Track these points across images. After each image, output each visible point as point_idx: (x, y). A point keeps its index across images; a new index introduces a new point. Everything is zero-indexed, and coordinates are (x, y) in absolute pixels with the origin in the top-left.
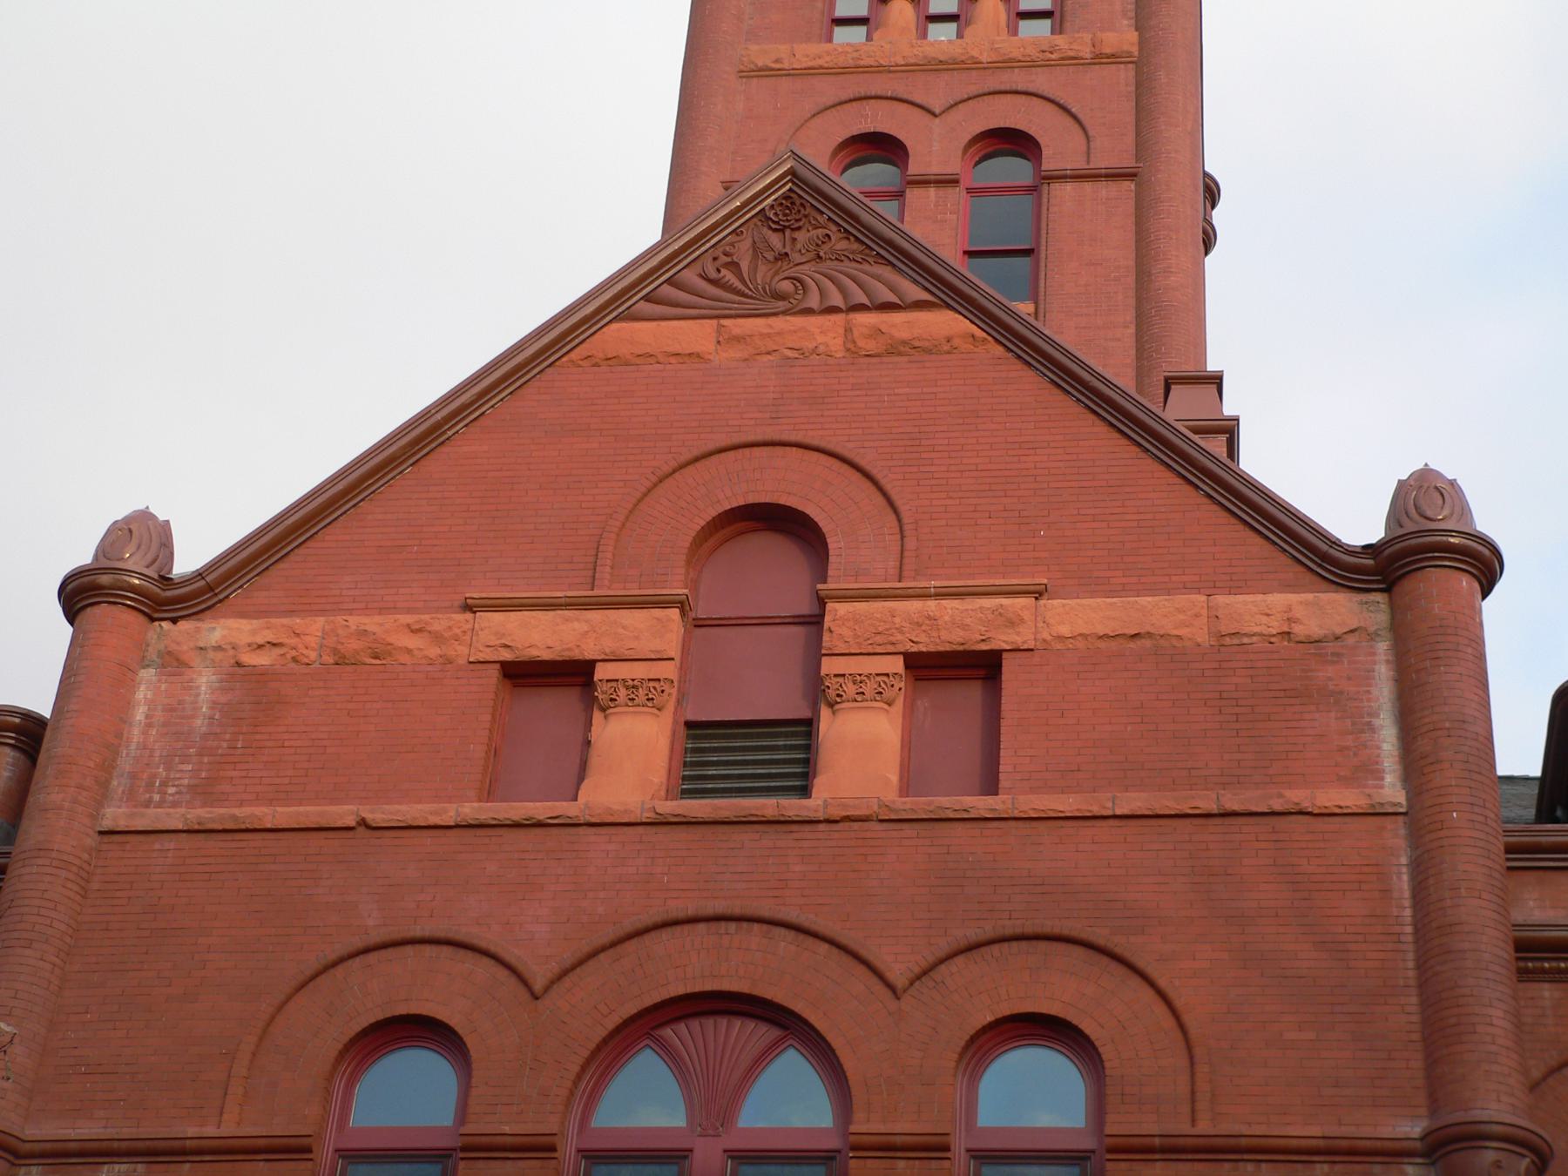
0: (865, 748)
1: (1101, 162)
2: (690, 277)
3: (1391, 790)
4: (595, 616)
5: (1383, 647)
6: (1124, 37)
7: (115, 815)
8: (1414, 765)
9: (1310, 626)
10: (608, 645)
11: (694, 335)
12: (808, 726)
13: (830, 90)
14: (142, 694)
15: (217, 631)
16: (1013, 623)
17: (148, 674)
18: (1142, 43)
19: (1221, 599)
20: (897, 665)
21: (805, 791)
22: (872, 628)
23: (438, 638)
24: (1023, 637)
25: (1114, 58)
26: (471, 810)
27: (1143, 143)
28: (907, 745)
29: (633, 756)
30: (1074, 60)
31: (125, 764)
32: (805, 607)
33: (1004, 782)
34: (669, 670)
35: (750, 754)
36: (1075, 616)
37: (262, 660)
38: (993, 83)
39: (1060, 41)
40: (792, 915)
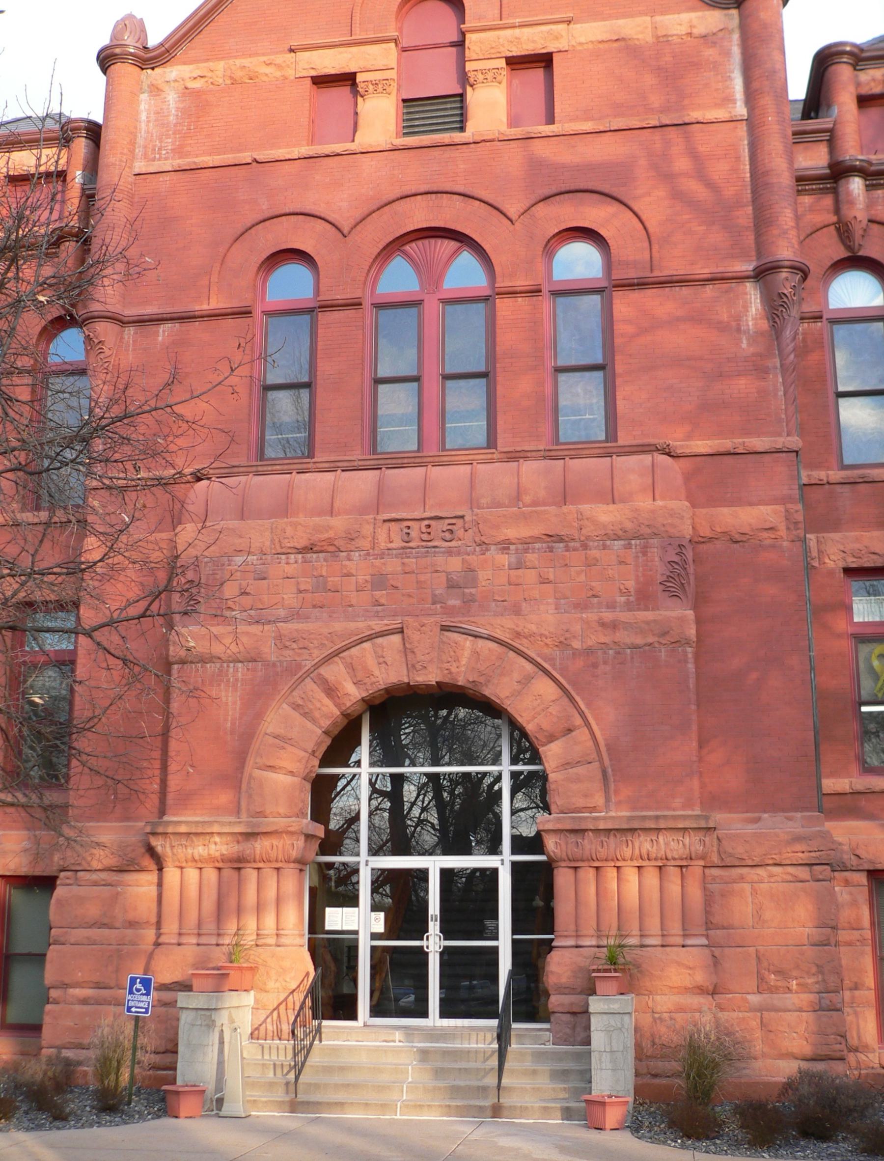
0: (490, 106)
3: (741, 110)
4: (354, 49)
7: (140, 166)
12: (462, 96)
14: (143, 107)
16: (557, 38)
17: (144, 97)
20: (502, 63)
21: (462, 129)
22: (488, 46)
23: (279, 67)
24: (563, 45)
28: (509, 103)
29: (379, 118)
31: (140, 141)
34: (393, 74)
35: (437, 112)
36: (588, 32)
37: (192, 85)
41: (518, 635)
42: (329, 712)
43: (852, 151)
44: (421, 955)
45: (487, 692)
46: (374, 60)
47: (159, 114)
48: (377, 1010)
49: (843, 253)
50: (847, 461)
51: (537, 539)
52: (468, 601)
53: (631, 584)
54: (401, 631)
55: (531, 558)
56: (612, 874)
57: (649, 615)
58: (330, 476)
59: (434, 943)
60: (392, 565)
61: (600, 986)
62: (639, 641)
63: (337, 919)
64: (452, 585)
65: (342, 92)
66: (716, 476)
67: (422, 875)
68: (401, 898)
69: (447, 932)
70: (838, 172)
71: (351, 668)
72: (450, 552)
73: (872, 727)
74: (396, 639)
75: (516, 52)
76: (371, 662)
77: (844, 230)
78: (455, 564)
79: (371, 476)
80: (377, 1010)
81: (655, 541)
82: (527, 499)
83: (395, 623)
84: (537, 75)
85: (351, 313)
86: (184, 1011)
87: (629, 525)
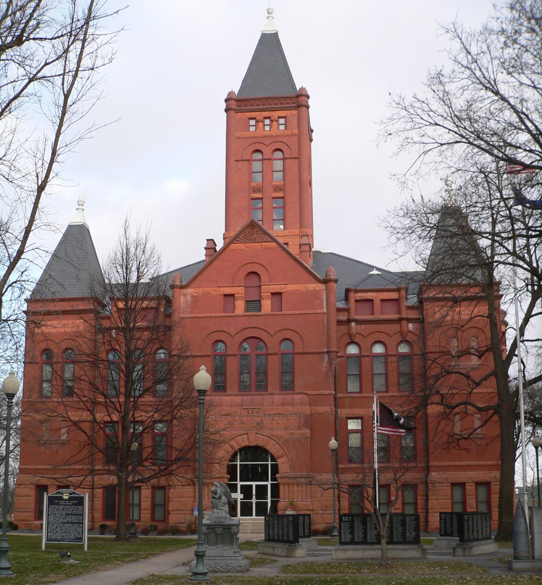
0: (267, 304)
1: (294, 156)
2: (241, 237)
3: (325, 310)
4: (234, 288)
5: (325, 291)
6: (296, 131)
7: (182, 315)
8: (328, 308)
9: (317, 289)
10: (236, 292)
11: (241, 246)
12: (260, 301)
13: (250, 141)
14: (182, 299)
15: (189, 291)
16: (283, 289)
17: (182, 296)
18: (299, 132)
19: (307, 285)
20: (270, 294)
21: (260, 311)
22: (267, 289)
23: (216, 291)
24: (284, 291)
25: (295, 135)
26: (222, 314)
27: (299, 152)
28: (271, 304)
29: (240, 305)
30: (288, 135)
31: (182, 309)
32: (258, 285)
33: (283, 310)
34: (243, 295)
35: (254, 304)
36: (290, 287)
37: (195, 294)
38: (276, 139)
39: (286, 131)
40: (260, 327)
41: (272, 435)
42: (232, 452)
43: (353, 316)
45: (266, 447)
46: (239, 291)
47: (186, 302)
49: (350, 341)
50: (349, 391)
51: (276, 414)
52: (262, 427)
53: (297, 425)
54: (247, 434)
55: (275, 418)
57: (300, 431)
58: (230, 397)
59: (254, 500)
60: (245, 419)
61: (288, 509)
62: (298, 437)
63: (233, 495)
64: (258, 424)
65: (231, 298)
66: (314, 401)
67: (251, 486)
68: (247, 491)
69: (257, 498)
70: (349, 321)
71: (236, 441)
72: (257, 416)
74: (246, 435)
76: (241, 440)
77: (350, 335)
78: (258, 419)
79: (240, 397)
81: (302, 415)
82: (275, 405)
83: (246, 432)
84: (278, 297)
85: (235, 357)
86: (480, 425)
87: (296, 411)
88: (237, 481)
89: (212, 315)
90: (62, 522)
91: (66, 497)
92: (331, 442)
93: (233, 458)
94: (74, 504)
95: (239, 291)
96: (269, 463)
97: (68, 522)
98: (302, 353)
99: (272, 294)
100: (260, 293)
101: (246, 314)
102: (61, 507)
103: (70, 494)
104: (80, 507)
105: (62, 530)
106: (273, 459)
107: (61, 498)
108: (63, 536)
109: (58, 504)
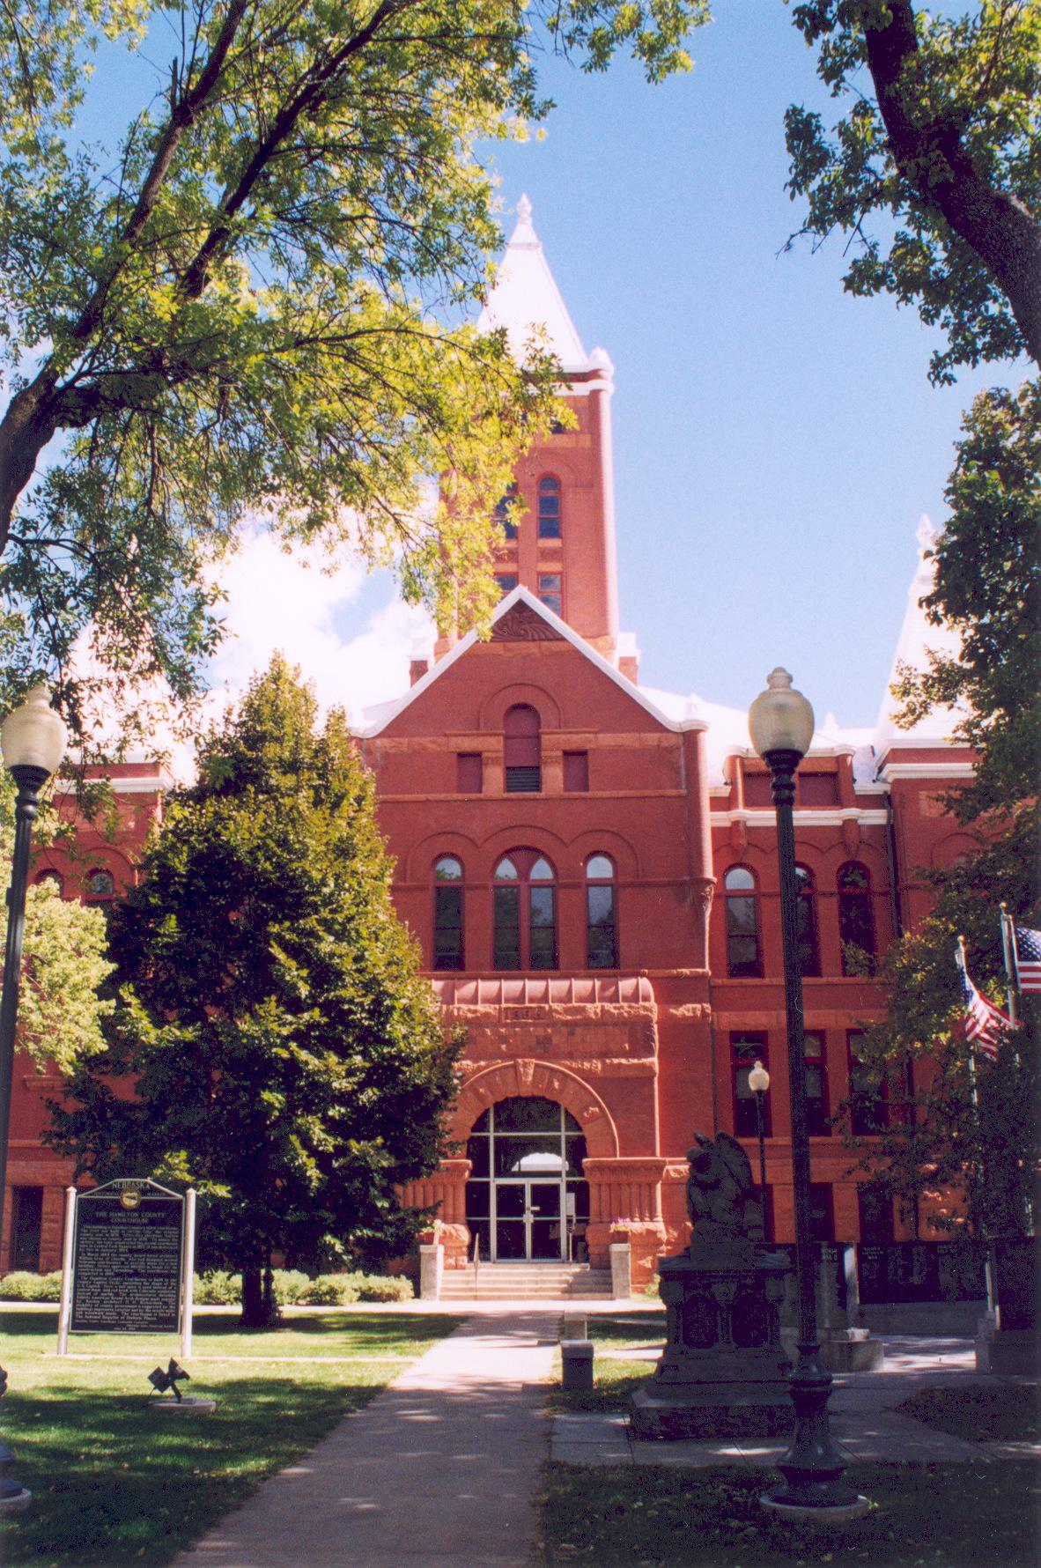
0: (554, 776)
22: (555, 741)
24: (593, 746)
28: (565, 776)
29: (494, 777)
34: (501, 755)
35: (524, 776)
36: (607, 740)
44: (521, 1226)
48: (534, 1255)
56: (450, 1191)
59: (528, 1219)
73: (504, 1116)
75: (568, 748)
80: (534, 1255)
88: (487, 1175)
89: (432, 797)
90: (117, 1275)
91: (129, 1201)
92: (752, 1075)
93: (481, 1124)
94: (152, 1222)
95: (492, 745)
96: (563, 1134)
97: (136, 1274)
98: (633, 885)
99: (566, 754)
100: (539, 750)
101: (506, 795)
102: (115, 1231)
103: (144, 1192)
104: (171, 1231)
105: (117, 1295)
106: (574, 1124)
107: (118, 1206)
108: (119, 1314)
109: (107, 1222)
